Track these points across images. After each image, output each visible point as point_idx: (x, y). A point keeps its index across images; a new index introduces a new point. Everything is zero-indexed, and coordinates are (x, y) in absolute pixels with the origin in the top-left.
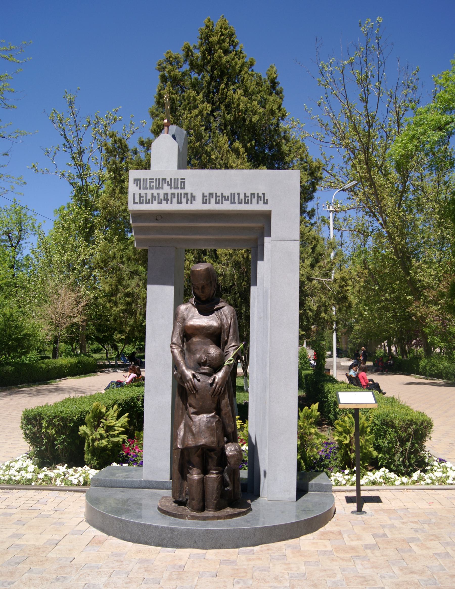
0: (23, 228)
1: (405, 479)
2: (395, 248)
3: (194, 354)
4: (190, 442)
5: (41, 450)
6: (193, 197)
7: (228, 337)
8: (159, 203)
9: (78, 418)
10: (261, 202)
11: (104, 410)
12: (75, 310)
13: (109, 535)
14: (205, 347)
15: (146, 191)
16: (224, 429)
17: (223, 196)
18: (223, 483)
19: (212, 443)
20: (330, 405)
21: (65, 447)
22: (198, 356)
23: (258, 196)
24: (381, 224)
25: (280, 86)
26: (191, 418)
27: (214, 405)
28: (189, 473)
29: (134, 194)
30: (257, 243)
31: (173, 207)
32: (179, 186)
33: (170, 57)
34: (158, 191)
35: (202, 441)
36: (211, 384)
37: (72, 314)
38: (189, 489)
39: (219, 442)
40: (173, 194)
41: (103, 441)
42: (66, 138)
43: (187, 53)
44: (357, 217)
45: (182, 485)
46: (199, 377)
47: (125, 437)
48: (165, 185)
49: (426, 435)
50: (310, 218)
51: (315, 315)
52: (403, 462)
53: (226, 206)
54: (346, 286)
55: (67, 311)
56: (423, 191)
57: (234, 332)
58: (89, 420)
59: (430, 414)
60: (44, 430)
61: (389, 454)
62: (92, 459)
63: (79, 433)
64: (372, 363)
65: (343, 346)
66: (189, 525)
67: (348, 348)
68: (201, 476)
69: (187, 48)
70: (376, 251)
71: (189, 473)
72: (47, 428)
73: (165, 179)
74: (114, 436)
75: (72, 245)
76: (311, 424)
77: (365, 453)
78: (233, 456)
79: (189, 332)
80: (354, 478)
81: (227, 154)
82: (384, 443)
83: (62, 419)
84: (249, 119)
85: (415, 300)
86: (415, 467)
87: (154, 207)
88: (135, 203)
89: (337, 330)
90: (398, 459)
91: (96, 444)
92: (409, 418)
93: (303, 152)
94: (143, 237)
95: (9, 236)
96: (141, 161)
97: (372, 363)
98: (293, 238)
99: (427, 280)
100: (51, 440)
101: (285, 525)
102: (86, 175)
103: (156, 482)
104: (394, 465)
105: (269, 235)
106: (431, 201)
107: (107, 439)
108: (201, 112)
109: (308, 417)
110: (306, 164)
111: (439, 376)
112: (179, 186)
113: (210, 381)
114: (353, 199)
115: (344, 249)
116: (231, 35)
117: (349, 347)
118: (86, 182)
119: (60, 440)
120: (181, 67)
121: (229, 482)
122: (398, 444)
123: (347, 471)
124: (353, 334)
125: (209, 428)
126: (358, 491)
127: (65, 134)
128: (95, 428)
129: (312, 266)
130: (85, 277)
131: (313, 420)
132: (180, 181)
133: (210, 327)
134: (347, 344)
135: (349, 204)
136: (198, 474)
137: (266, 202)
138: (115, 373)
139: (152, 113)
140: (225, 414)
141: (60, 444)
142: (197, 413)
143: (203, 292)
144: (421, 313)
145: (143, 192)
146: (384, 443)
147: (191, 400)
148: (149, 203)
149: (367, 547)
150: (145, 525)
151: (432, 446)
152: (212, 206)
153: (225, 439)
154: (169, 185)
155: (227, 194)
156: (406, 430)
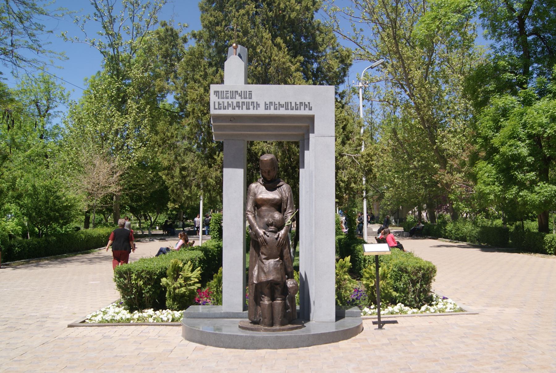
0: (52, 96)
1: (415, 310)
2: (422, 118)
3: (263, 218)
4: (263, 279)
5: (131, 298)
6: (258, 105)
7: (287, 206)
8: (233, 109)
9: (160, 272)
11: (181, 265)
12: (112, 180)
13: (206, 345)
14: (271, 213)
15: (223, 100)
16: (286, 269)
17: (279, 104)
18: (285, 307)
19: (278, 278)
20: (360, 262)
21: (150, 296)
22: (266, 220)
23: (305, 105)
24: (408, 95)
26: (263, 262)
27: (279, 253)
28: (261, 300)
29: (214, 102)
30: (304, 137)
31: (243, 112)
32: (248, 96)
34: (232, 100)
35: (271, 278)
36: (277, 239)
37: (107, 185)
38: (262, 312)
39: (282, 278)
41: (182, 289)
42: (96, 7)
44: (385, 89)
45: (256, 310)
46: (268, 234)
47: (199, 285)
48: (237, 96)
49: (431, 278)
50: (342, 99)
51: (347, 185)
52: (415, 298)
53: (282, 112)
54: (372, 161)
55: (103, 182)
56: (448, 63)
57: (291, 202)
58: (170, 274)
59: (434, 263)
61: (404, 293)
62: (173, 304)
63: (161, 284)
64: (402, 228)
65: (375, 212)
66: (262, 333)
67: (379, 214)
68: (271, 302)
70: (405, 120)
71: (261, 300)
72: (136, 280)
73: (237, 92)
74: (190, 285)
75: (105, 114)
76: (345, 272)
77: (386, 293)
78: (292, 288)
79: (259, 203)
80: (377, 310)
81: (271, 50)
82: (401, 285)
83: (148, 273)
84: (287, 16)
85: (440, 168)
86: (424, 302)
87: (230, 112)
88: (215, 109)
89: (366, 197)
90: (411, 296)
91: (177, 291)
92: (418, 265)
93: (334, 42)
95: (37, 105)
96: (194, 52)
97: (402, 228)
98: (330, 135)
99: (451, 149)
100: (140, 290)
101: (329, 333)
102: (118, 44)
103: (233, 313)
104: (408, 301)
105: (313, 132)
106: (456, 72)
107: (185, 288)
108: (248, 13)
109: (342, 267)
110: (337, 53)
111: (463, 239)
112: (248, 96)
113: (276, 236)
114: (382, 71)
115: (374, 117)
117: (381, 213)
118: (118, 52)
122: (411, 285)
123: (372, 307)
124: (383, 201)
125: (275, 268)
126: (379, 318)
127: (96, 3)
128: (176, 279)
129: (343, 143)
130: (118, 147)
131: (346, 269)
132: (248, 93)
133: (275, 199)
134: (379, 211)
135: (378, 75)
136: (268, 301)
137: (310, 109)
138: (152, 243)
139: (202, 8)
140: (287, 259)
141: (148, 292)
142: (267, 259)
143: (269, 175)
144: (446, 180)
145: (221, 101)
146: (400, 284)
147: (263, 250)
148: (225, 109)
149: (383, 345)
150: (233, 335)
151: (437, 287)
152: (272, 112)
153: (286, 276)
154: (240, 96)
155: (282, 103)
156: (416, 274)
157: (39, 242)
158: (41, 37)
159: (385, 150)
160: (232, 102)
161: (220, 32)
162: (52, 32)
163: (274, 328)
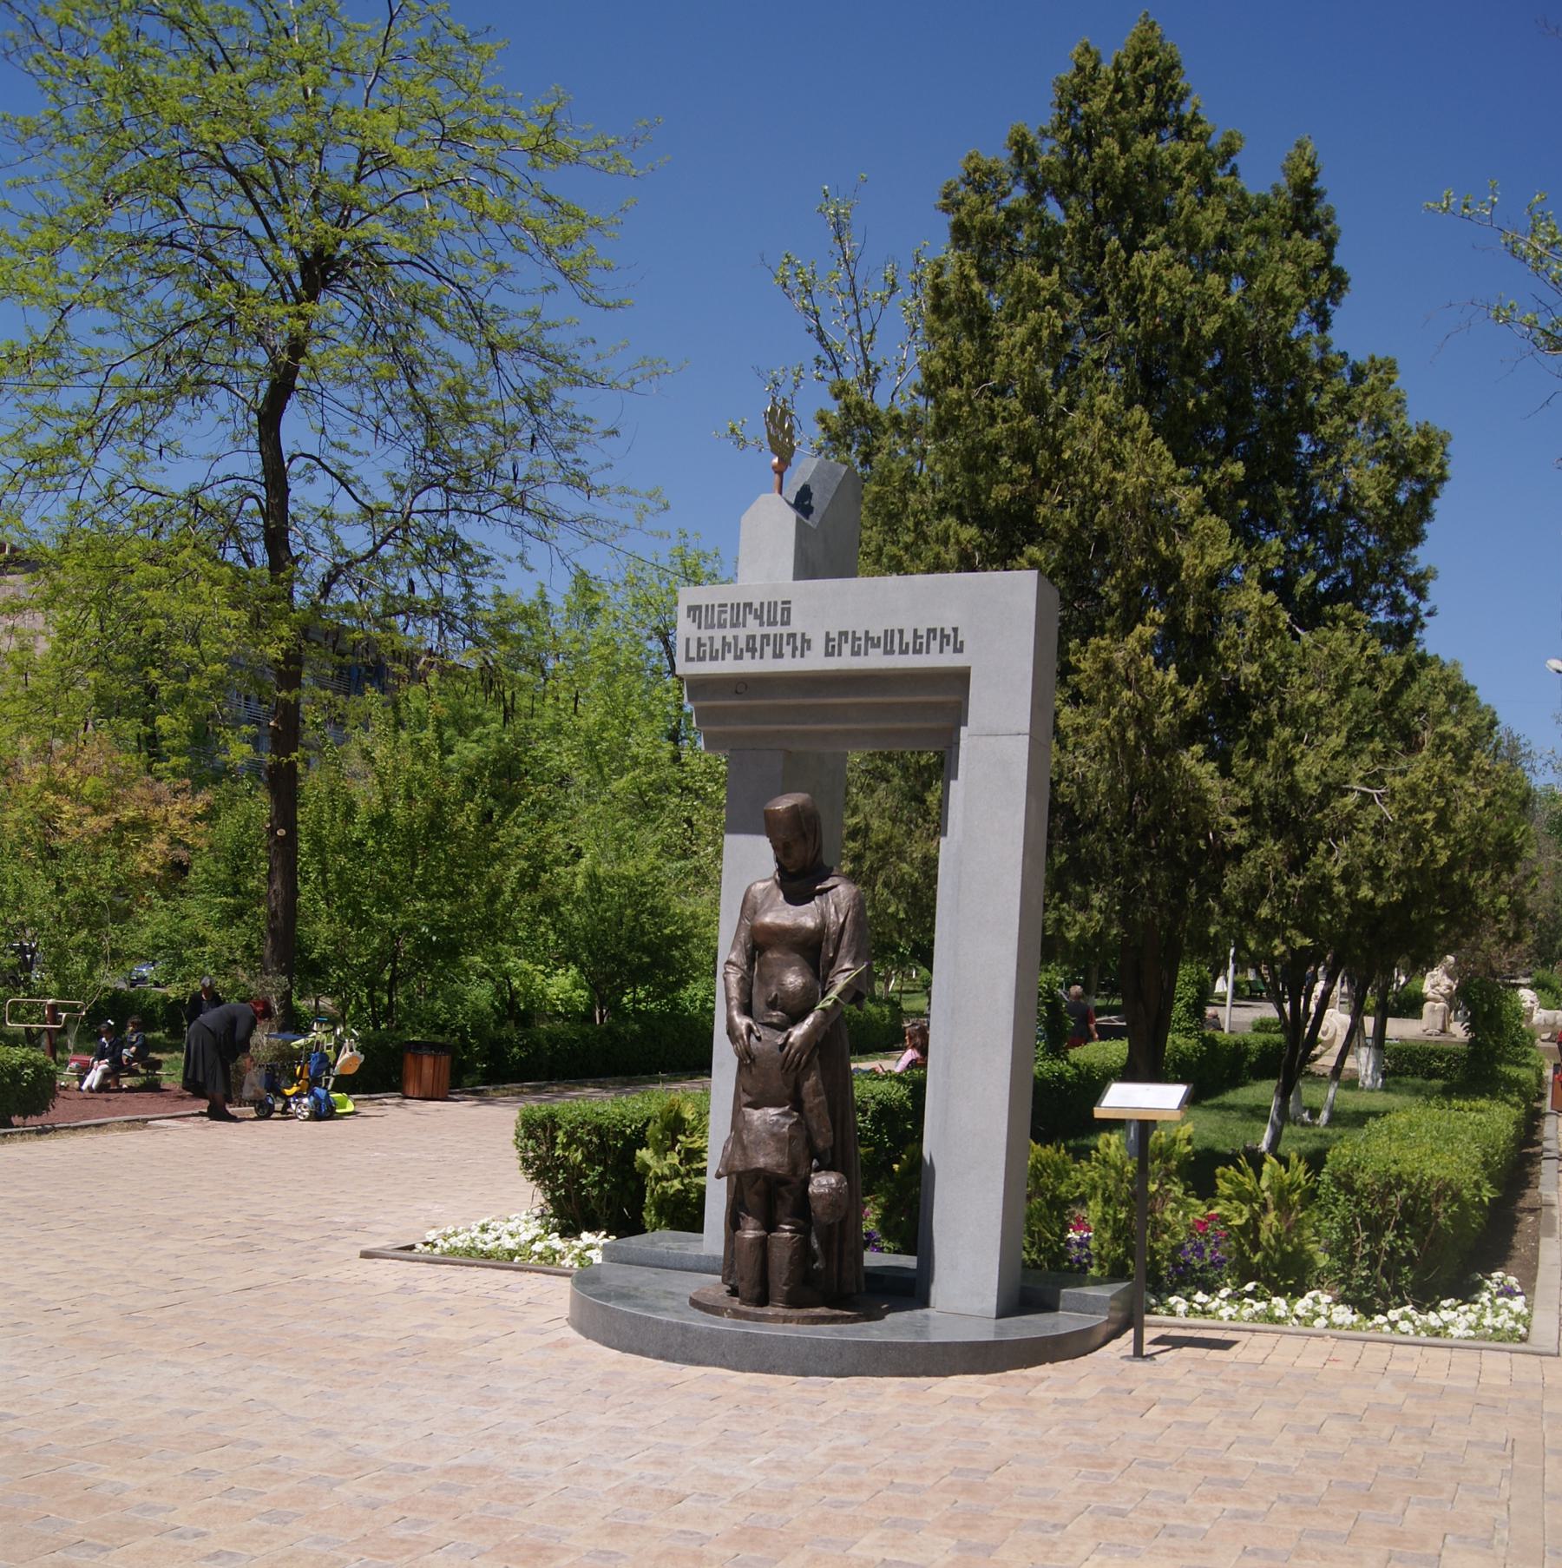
6: (807, 642)
10: (949, 649)
15: (710, 633)
18: (803, 1253)
19: (779, 1166)
23: (943, 636)
25: (1328, 200)
27: (788, 1091)
33: (976, 170)
34: (735, 631)
36: (782, 1047)
39: (794, 1167)
40: (765, 637)
42: (821, 338)
43: (1019, 155)
48: (750, 618)
53: (875, 660)
57: (852, 940)
60: (558, 1152)
68: (762, 1233)
69: (1016, 143)
72: (566, 1147)
78: (821, 1196)
83: (598, 1130)
87: (727, 666)
88: (689, 659)
94: (716, 729)
100: (575, 1173)
113: (780, 1041)
116: (1171, 68)
119: (593, 1176)
120: (1004, 195)
121: (819, 1252)
127: (819, 327)
132: (780, 607)
137: (959, 649)
140: (811, 1110)
141: (593, 1185)
145: (705, 634)
148: (716, 658)
152: (845, 662)
153: (815, 1162)
154: (759, 617)
155: (876, 632)
157: (584, 1037)
158: (591, 454)
159: (1488, 773)
160: (736, 638)
161: (959, 404)
162: (614, 432)
163: (769, 1311)
